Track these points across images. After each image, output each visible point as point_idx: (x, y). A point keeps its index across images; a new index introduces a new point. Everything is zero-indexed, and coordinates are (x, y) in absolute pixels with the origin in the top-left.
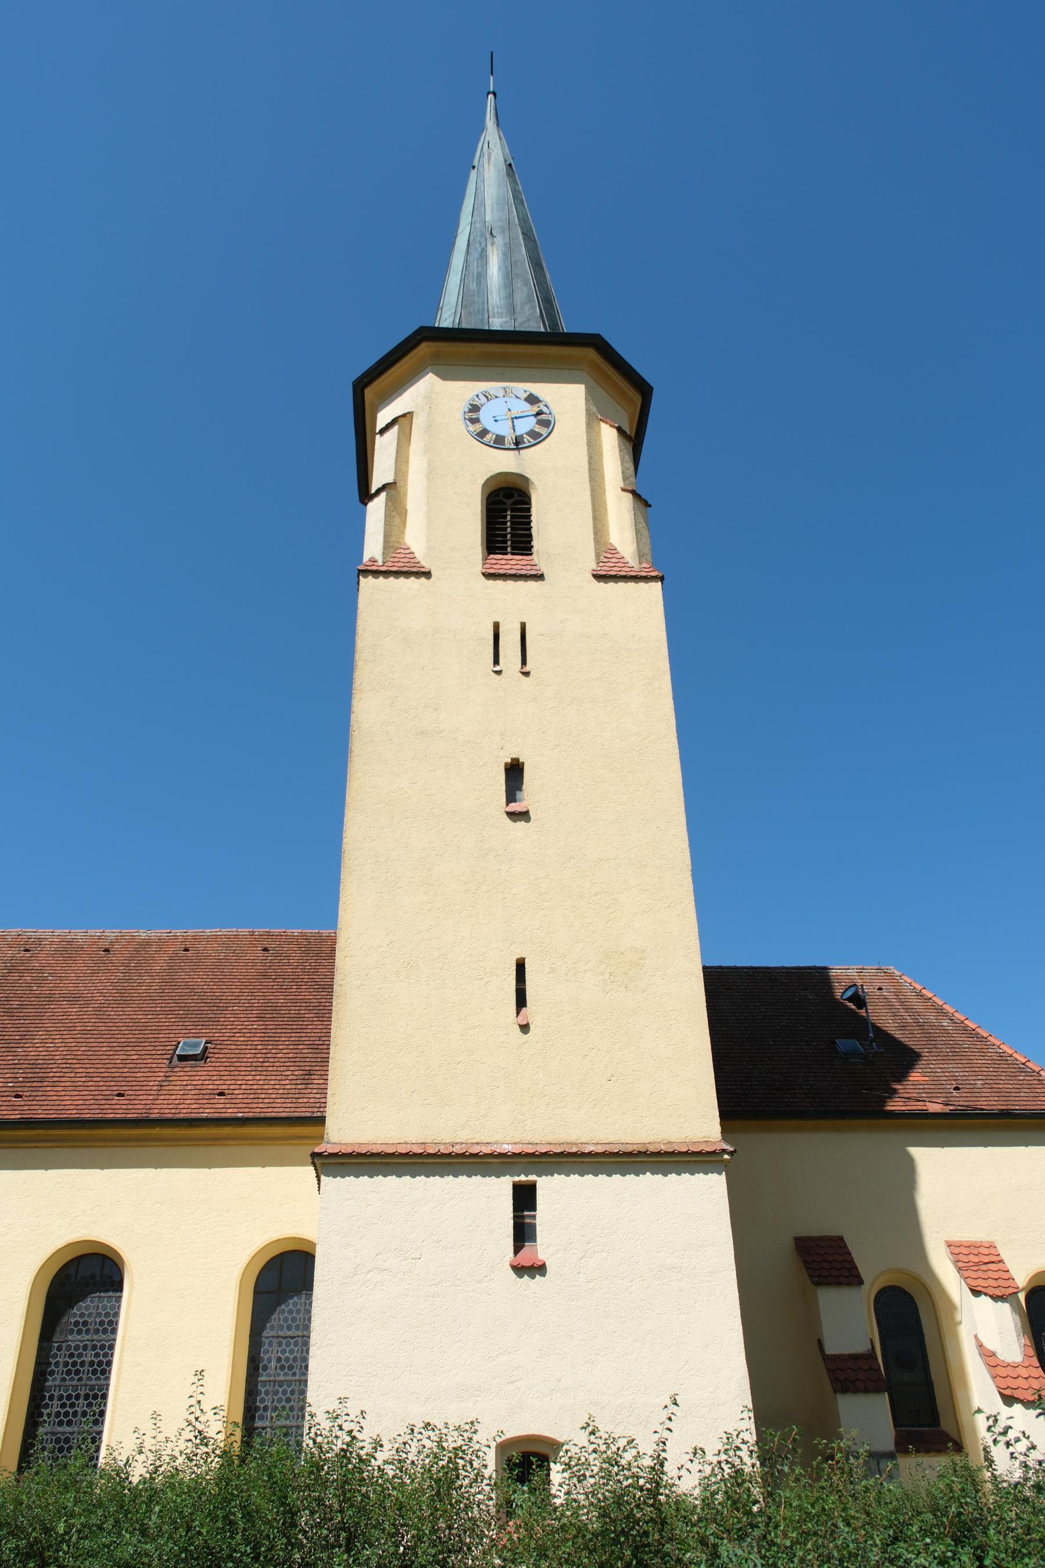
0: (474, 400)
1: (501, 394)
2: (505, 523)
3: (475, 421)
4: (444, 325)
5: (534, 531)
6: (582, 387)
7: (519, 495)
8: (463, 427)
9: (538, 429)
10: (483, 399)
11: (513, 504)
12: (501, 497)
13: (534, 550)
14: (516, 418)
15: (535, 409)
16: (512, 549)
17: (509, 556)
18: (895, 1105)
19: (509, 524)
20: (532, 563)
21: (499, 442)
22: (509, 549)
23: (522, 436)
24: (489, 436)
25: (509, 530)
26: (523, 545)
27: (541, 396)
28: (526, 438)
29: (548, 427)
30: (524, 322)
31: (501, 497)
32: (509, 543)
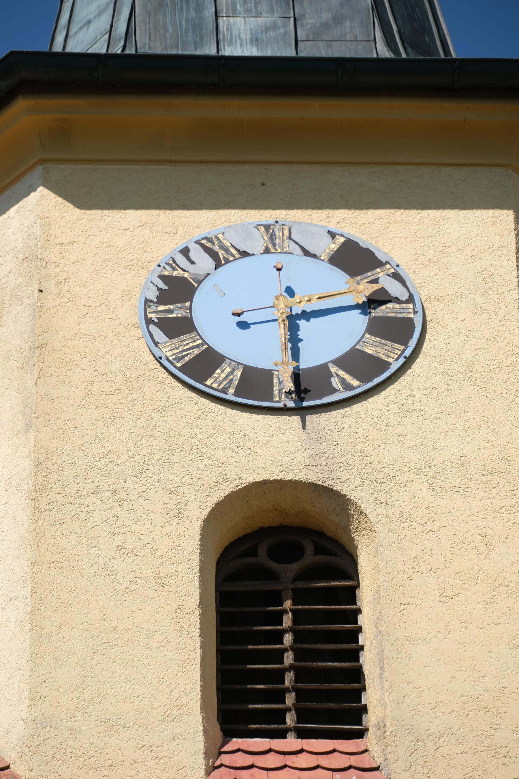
0: (174, 264)
1: (257, 243)
2: (278, 637)
3: (179, 327)
4: (75, 46)
5: (368, 661)
6: (507, 217)
7: (319, 550)
8: (141, 348)
9: (373, 347)
10: (204, 262)
11: (301, 576)
12: (263, 558)
13: (371, 720)
14: (306, 315)
15: (364, 289)
16: (303, 716)
17: (292, 742)
18: (345, 239)
19: (288, 639)
20: (364, 761)
21: (252, 391)
22: (290, 720)
23: (322, 371)
24: (221, 374)
25: (289, 658)
26: (335, 703)
27: (381, 249)
28: (339, 376)
29: (405, 343)
30: (326, 26)
31: (263, 558)
32: (290, 699)
